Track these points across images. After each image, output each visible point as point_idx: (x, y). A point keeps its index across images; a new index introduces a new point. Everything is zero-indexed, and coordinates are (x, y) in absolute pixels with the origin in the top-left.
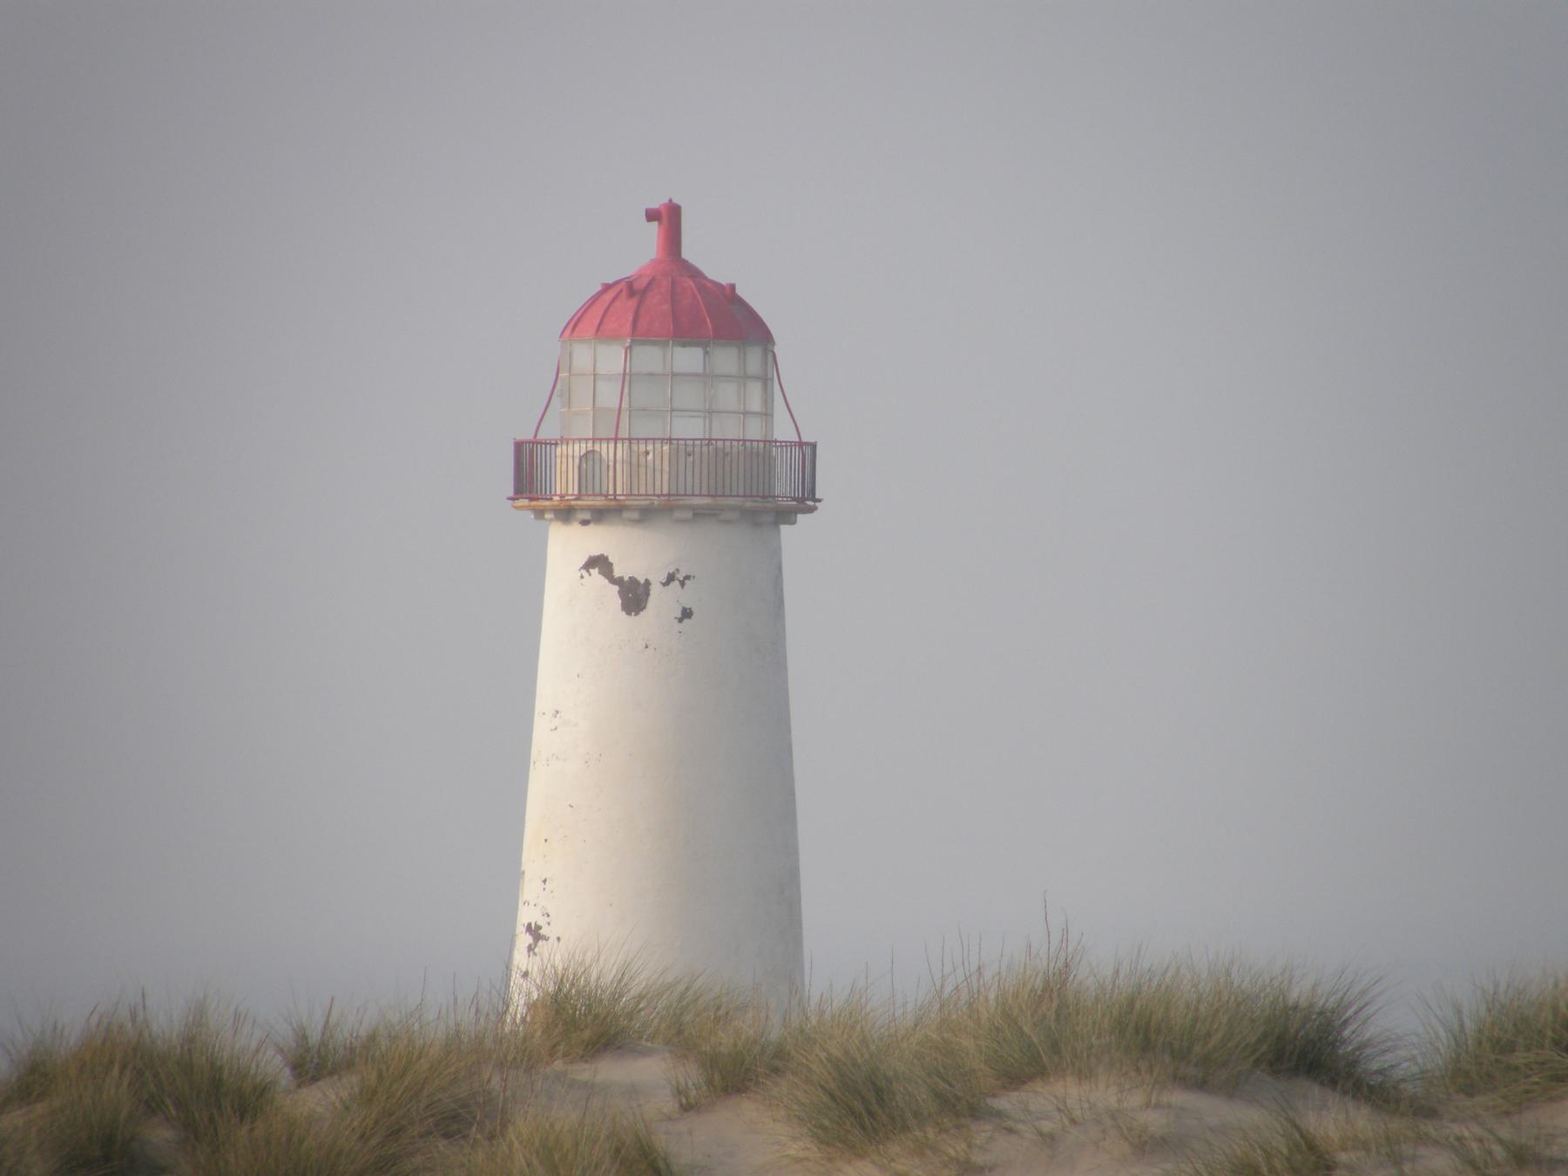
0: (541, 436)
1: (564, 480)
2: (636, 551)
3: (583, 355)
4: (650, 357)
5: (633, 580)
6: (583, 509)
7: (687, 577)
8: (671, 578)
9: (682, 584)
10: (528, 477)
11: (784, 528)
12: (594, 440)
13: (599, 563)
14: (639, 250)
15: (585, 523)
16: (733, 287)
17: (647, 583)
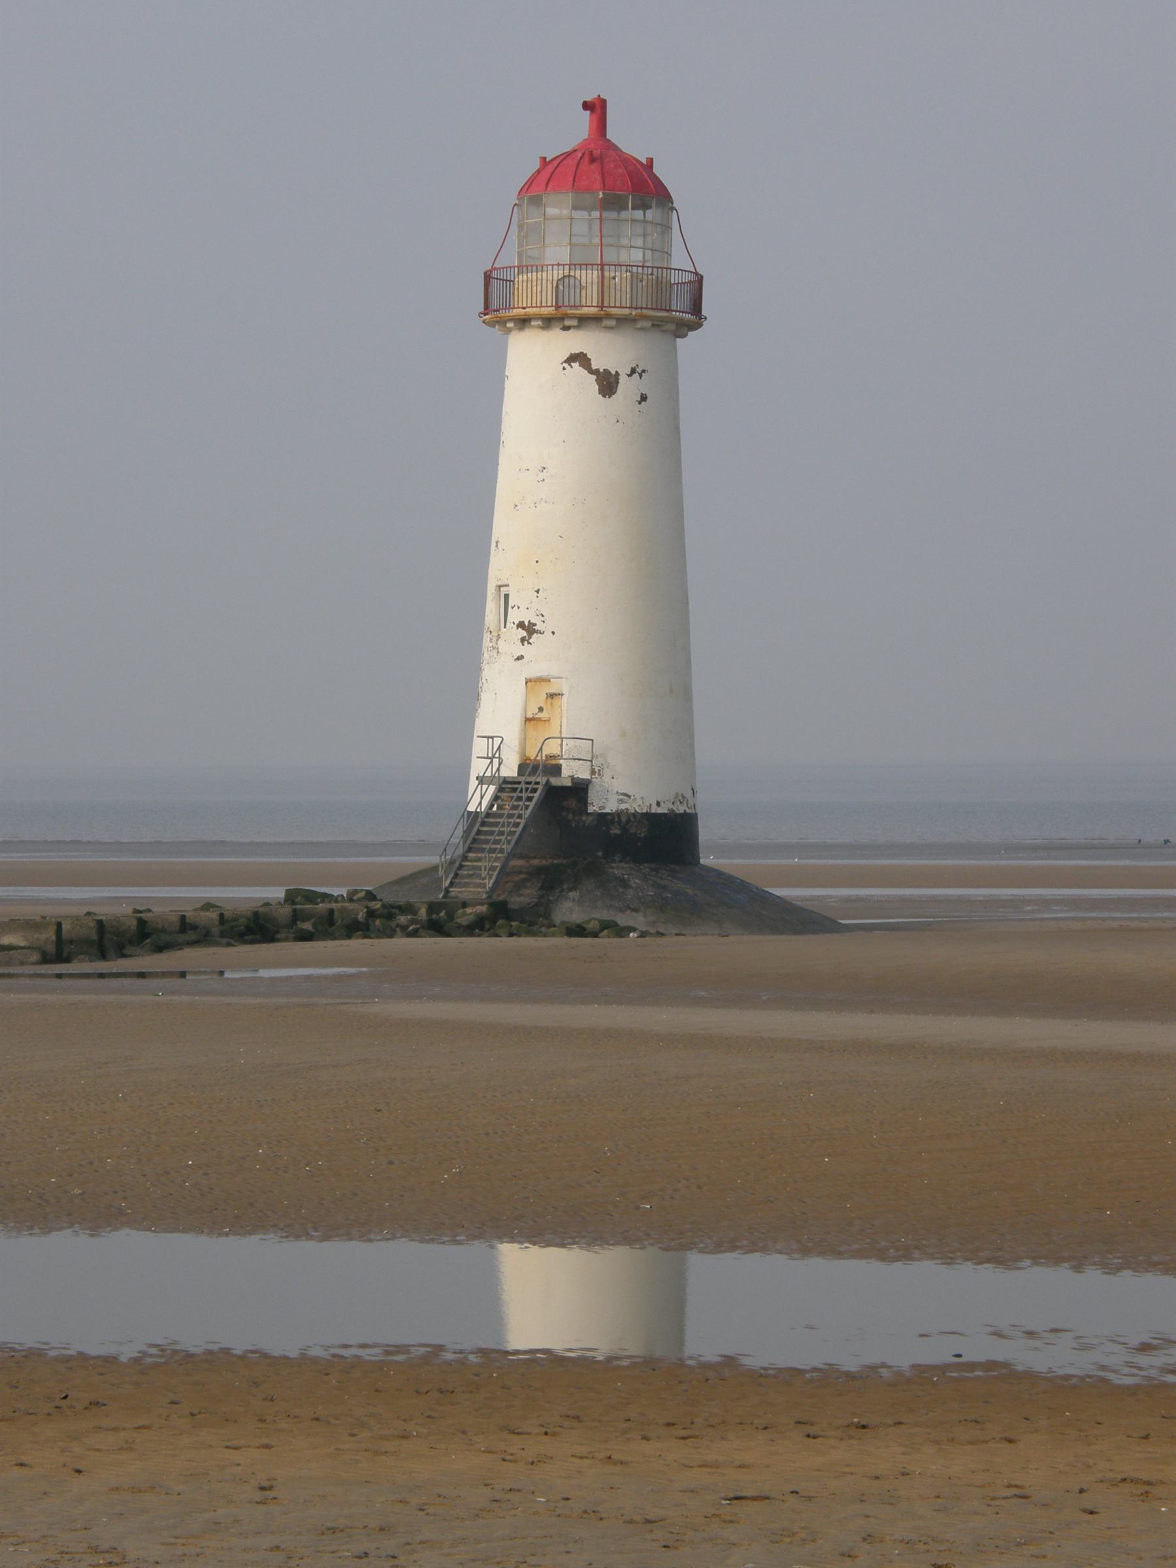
1: (533, 293)
2: (608, 350)
7: (643, 371)
8: (633, 371)
9: (641, 376)
12: (643, 267)
13: (579, 358)
14: (575, 131)
16: (650, 161)
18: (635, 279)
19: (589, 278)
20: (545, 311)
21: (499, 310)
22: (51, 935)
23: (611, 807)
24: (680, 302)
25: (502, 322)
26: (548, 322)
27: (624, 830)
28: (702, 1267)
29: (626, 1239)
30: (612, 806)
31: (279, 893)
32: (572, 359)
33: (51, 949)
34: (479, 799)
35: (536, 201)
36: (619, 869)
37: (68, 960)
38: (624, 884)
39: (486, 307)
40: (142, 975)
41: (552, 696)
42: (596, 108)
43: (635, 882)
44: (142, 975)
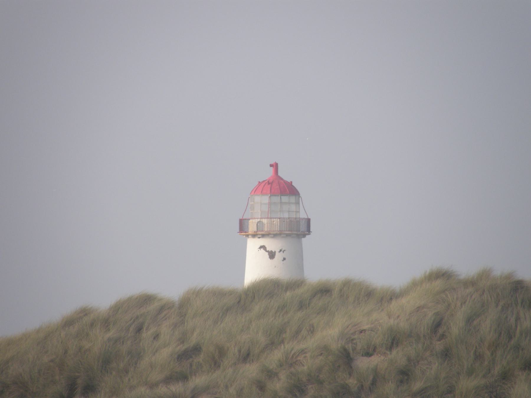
0: (244, 218)
1: (252, 227)
2: (272, 244)
3: (258, 199)
4: (276, 199)
5: (271, 251)
6: (259, 234)
8: (281, 251)
10: (242, 226)
11: (303, 239)
13: (263, 247)
14: (269, 173)
15: (259, 238)
16: (291, 182)
17: (275, 252)
24: (303, 228)
32: (261, 247)
42: (275, 166)
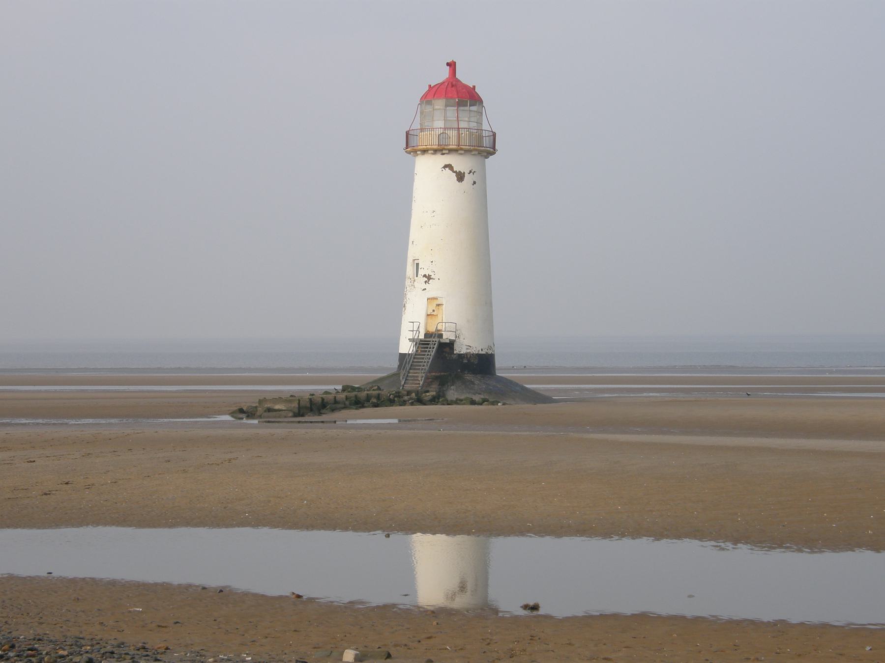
2: (461, 163)
14: (444, 74)
16: (474, 87)
18: (471, 134)
19: (453, 134)
20: (435, 147)
21: (412, 147)
22: (296, 405)
23: (463, 351)
24: (486, 142)
25: (415, 152)
26: (435, 151)
27: (469, 360)
28: (503, 547)
29: (469, 533)
30: (464, 351)
31: (339, 387)
32: (446, 166)
33: (296, 410)
34: (406, 347)
35: (429, 103)
36: (469, 377)
37: (303, 416)
38: (473, 383)
39: (407, 145)
40: (323, 422)
41: (438, 305)
42: (452, 65)
43: (477, 382)
44: (323, 422)
